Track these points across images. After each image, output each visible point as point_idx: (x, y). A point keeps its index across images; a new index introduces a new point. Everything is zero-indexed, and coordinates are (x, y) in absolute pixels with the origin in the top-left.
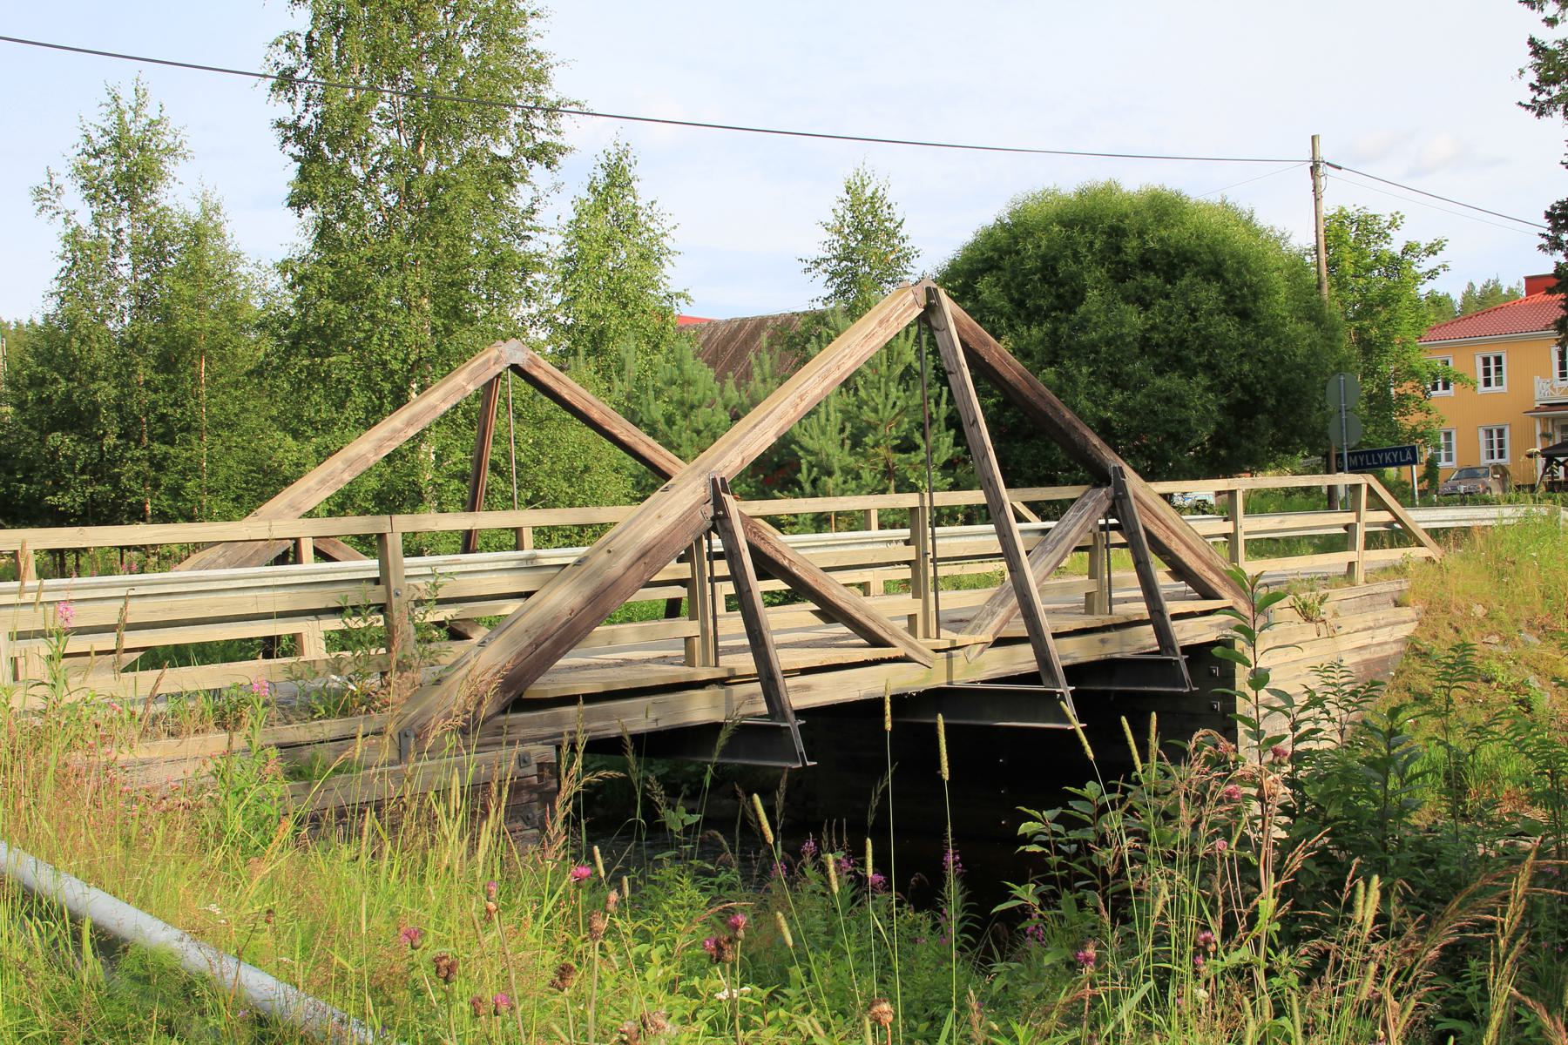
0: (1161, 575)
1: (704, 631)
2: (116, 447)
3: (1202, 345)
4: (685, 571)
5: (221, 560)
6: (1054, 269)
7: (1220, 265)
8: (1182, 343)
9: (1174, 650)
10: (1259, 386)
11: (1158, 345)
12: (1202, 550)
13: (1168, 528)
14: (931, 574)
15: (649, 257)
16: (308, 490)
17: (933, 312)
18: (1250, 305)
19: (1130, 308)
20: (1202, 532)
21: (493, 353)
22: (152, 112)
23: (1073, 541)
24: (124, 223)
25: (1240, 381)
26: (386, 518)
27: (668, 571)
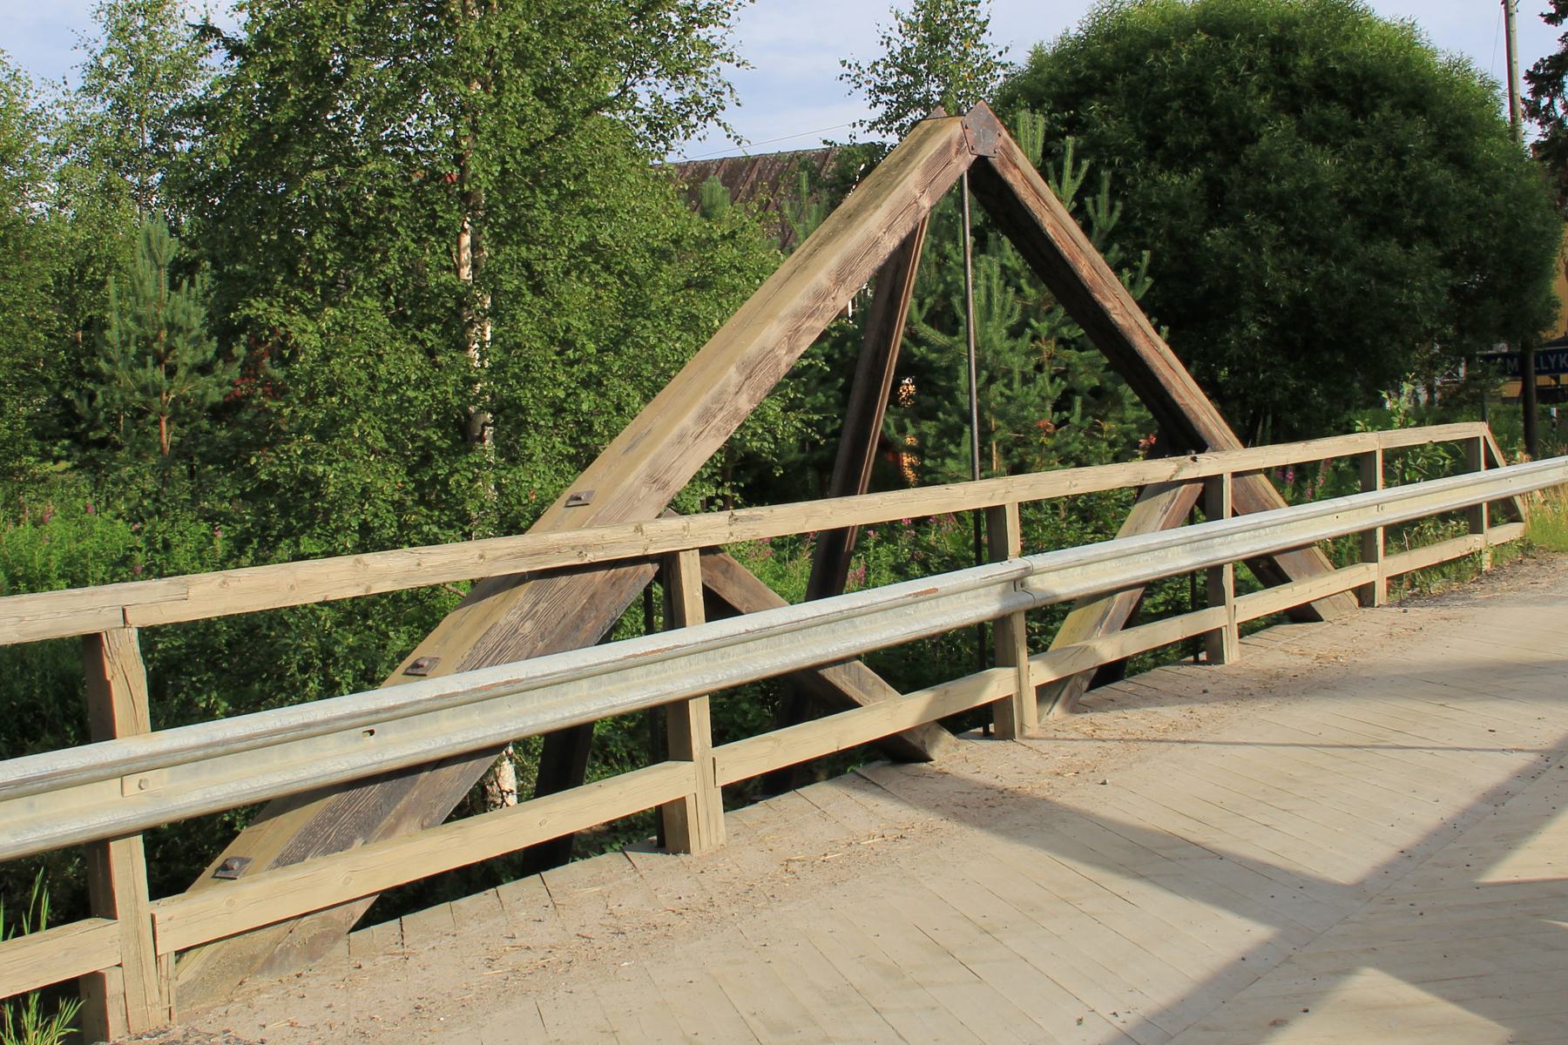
16: (681, 437)
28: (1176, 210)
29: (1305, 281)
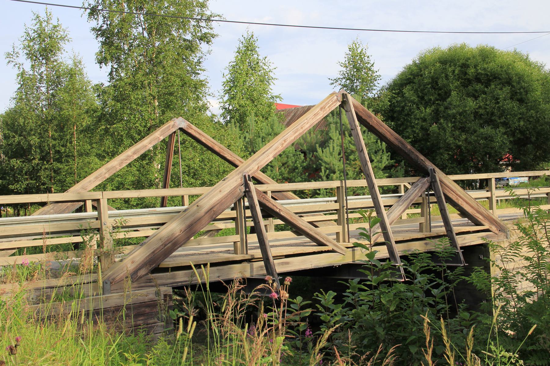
0: (454, 216)
1: (242, 239)
2: (38, 164)
3: (501, 114)
4: (234, 214)
5: (52, 211)
6: (437, 83)
7: (511, 79)
8: (493, 114)
9: (457, 248)
10: (528, 132)
11: (482, 115)
12: (474, 204)
13: (457, 195)
14: (346, 217)
15: (265, 80)
16: (90, 181)
17: (345, 104)
18: (524, 96)
19: (469, 99)
20: (474, 196)
21: (171, 123)
22: (54, 22)
23: (412, 200)
24: (43, 69)
25: (519, 130)
26: (101, 192)
27: (225, 214)
28: (424, 120)
29: (459, 141)
